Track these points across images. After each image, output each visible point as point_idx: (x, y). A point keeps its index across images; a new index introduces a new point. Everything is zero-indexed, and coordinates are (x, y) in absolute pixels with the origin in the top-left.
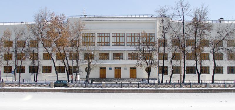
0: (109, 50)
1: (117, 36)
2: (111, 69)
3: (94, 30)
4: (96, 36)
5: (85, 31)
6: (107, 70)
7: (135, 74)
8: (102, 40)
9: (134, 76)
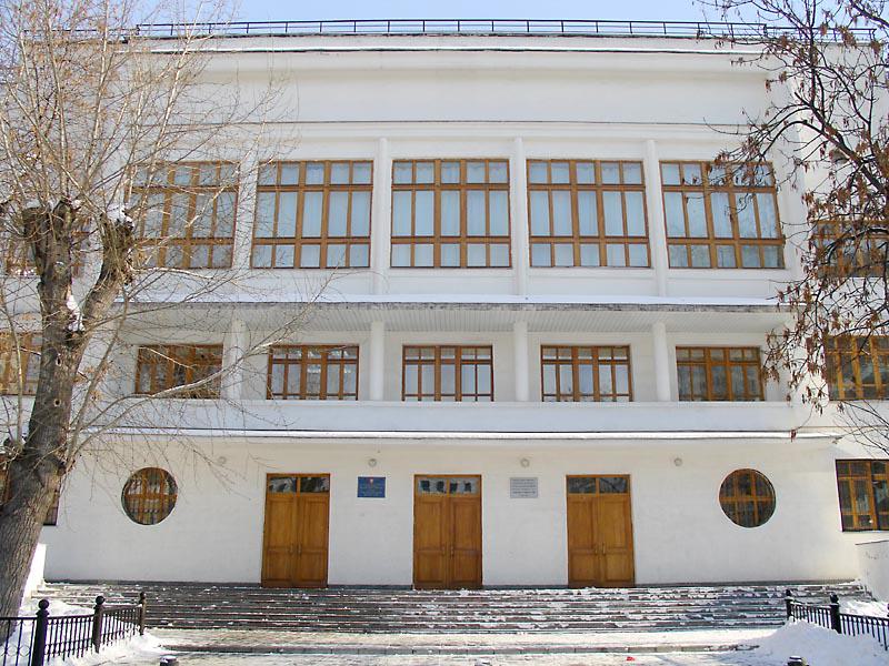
0: (369, 305)
1: (438, 187)
2: (362, 481)
3: (375, 131)
4: (249, 183)
5: (297, 140)
6: (342, 497)
7: (619, 540)
8: (733, 219)
9: (613, 567)
